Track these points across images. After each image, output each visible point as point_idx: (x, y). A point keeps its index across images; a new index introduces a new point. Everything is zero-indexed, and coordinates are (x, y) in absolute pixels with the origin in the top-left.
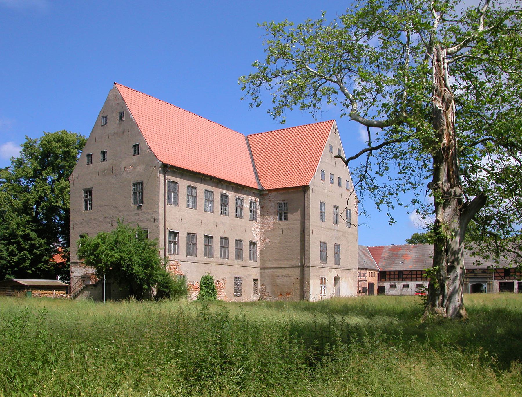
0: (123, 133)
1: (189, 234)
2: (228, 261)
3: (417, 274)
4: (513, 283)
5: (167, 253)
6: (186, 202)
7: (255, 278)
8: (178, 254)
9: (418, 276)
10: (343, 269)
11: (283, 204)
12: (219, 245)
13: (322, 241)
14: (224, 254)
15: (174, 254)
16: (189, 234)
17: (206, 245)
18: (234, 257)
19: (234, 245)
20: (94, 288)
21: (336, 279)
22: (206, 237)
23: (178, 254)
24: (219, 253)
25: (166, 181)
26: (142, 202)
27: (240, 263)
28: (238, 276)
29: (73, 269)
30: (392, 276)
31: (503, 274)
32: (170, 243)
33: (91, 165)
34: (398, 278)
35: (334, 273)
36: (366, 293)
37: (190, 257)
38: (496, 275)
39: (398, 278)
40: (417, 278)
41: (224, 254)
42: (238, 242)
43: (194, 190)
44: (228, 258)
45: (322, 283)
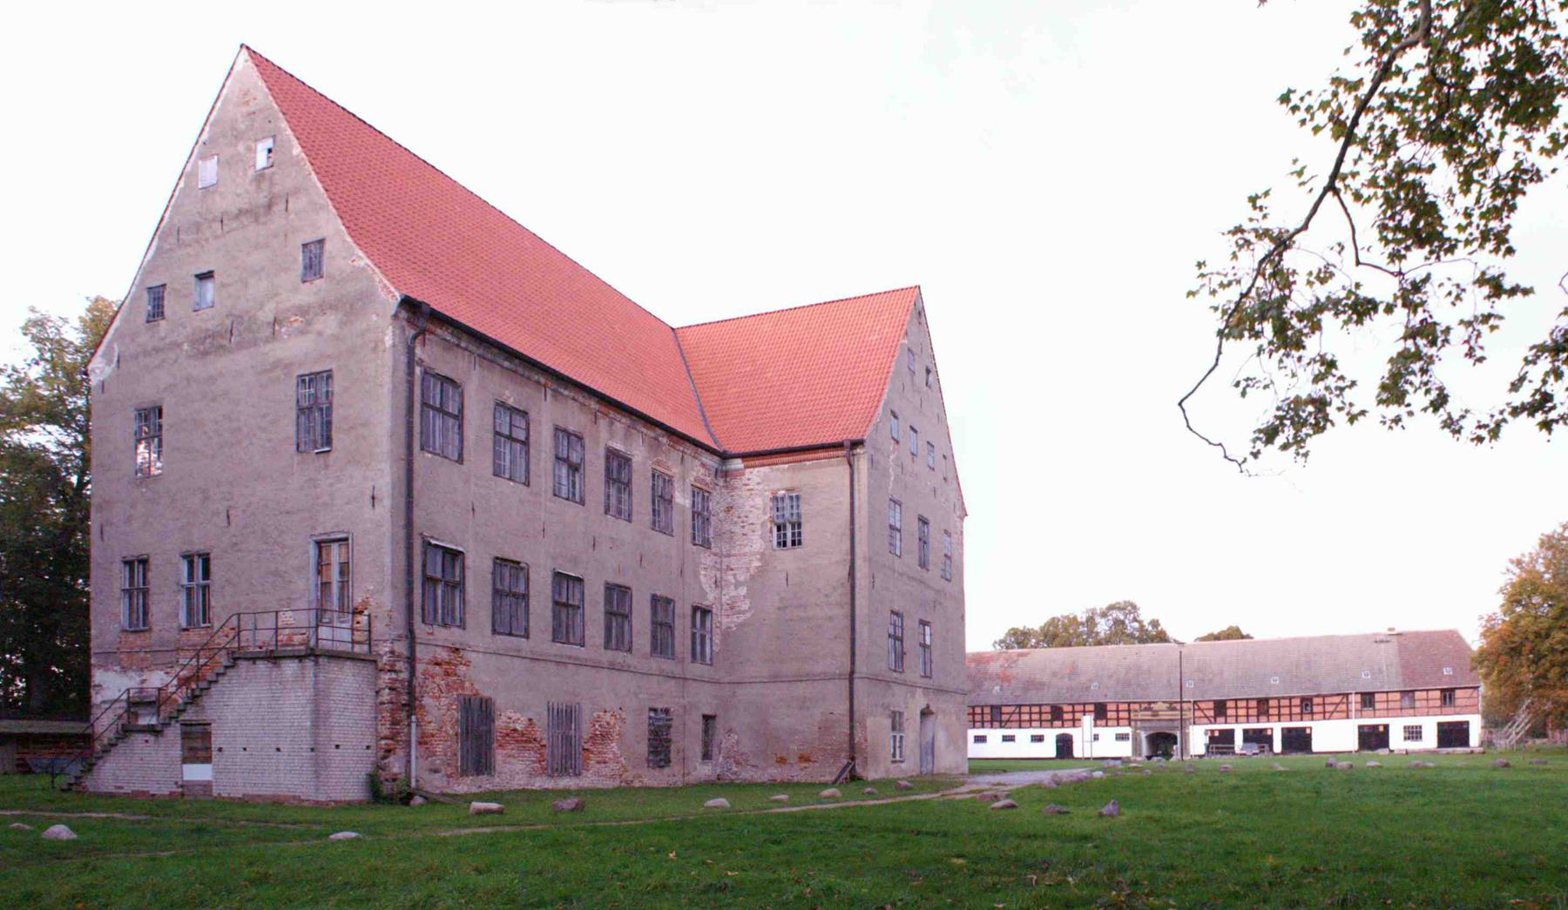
0: (269, 206)
1: (610, 588)
2: (629, 659)
3: (1040, 713)
4: (1232, 731)
5: (417, 618)
6: (491, 454)
7: (708, 712)
8: (463, 626)
9: (1122, 715)
10: (940, 691)
11: (787, 501)
12: (601, 607)
13: (896, 608)
14: (616, 635)
15: (445, 625)
16: (610, 588)
17: (556, 603)
18: (648, 648)
19: (648, 612)
20: (151, 738)
21: (926, 713)
22: (558, 576)
23: (463, 626)
24: (602, 633)
25: (418, 370)
26: (329, 441)
27: (664, 667)
28: (659, 706)
29: (98, 676)
30: (978, 718)
31: (1211, 713)
32: (428, 580)
33: (163, 323)
34: (992, 721)
35: (920, 702)
37: (503, 641)
38: (1198, 713)
39: (992, 721)
40: (1031, 721)
41: (616, 635)
42: (660, 604)
43: (519, 421)
44: (630, 650)
45: (894, 728)
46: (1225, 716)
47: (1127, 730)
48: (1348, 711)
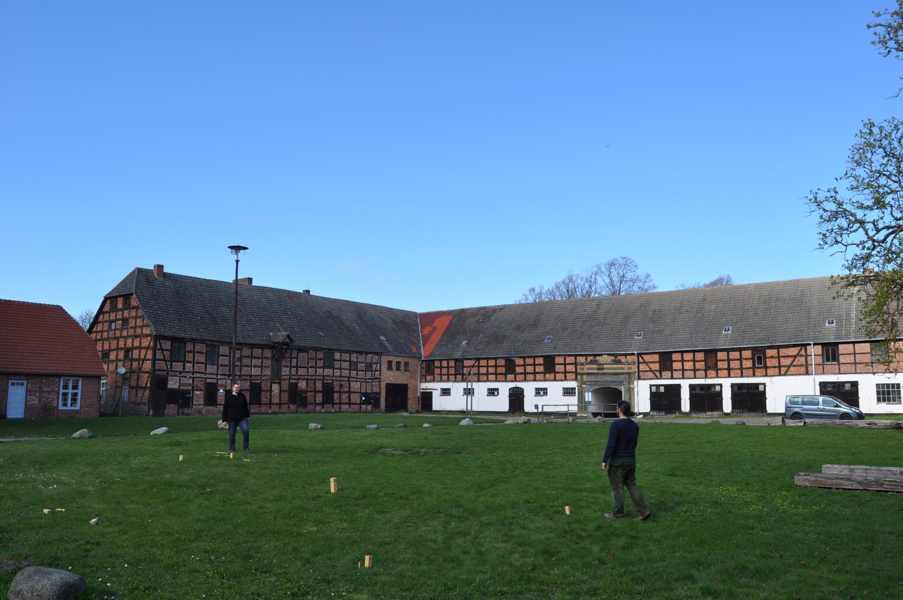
4: (678, 387)
36: (377, 405)
46: (672, 370)
47: (573, 384)
48: (807, 365)
